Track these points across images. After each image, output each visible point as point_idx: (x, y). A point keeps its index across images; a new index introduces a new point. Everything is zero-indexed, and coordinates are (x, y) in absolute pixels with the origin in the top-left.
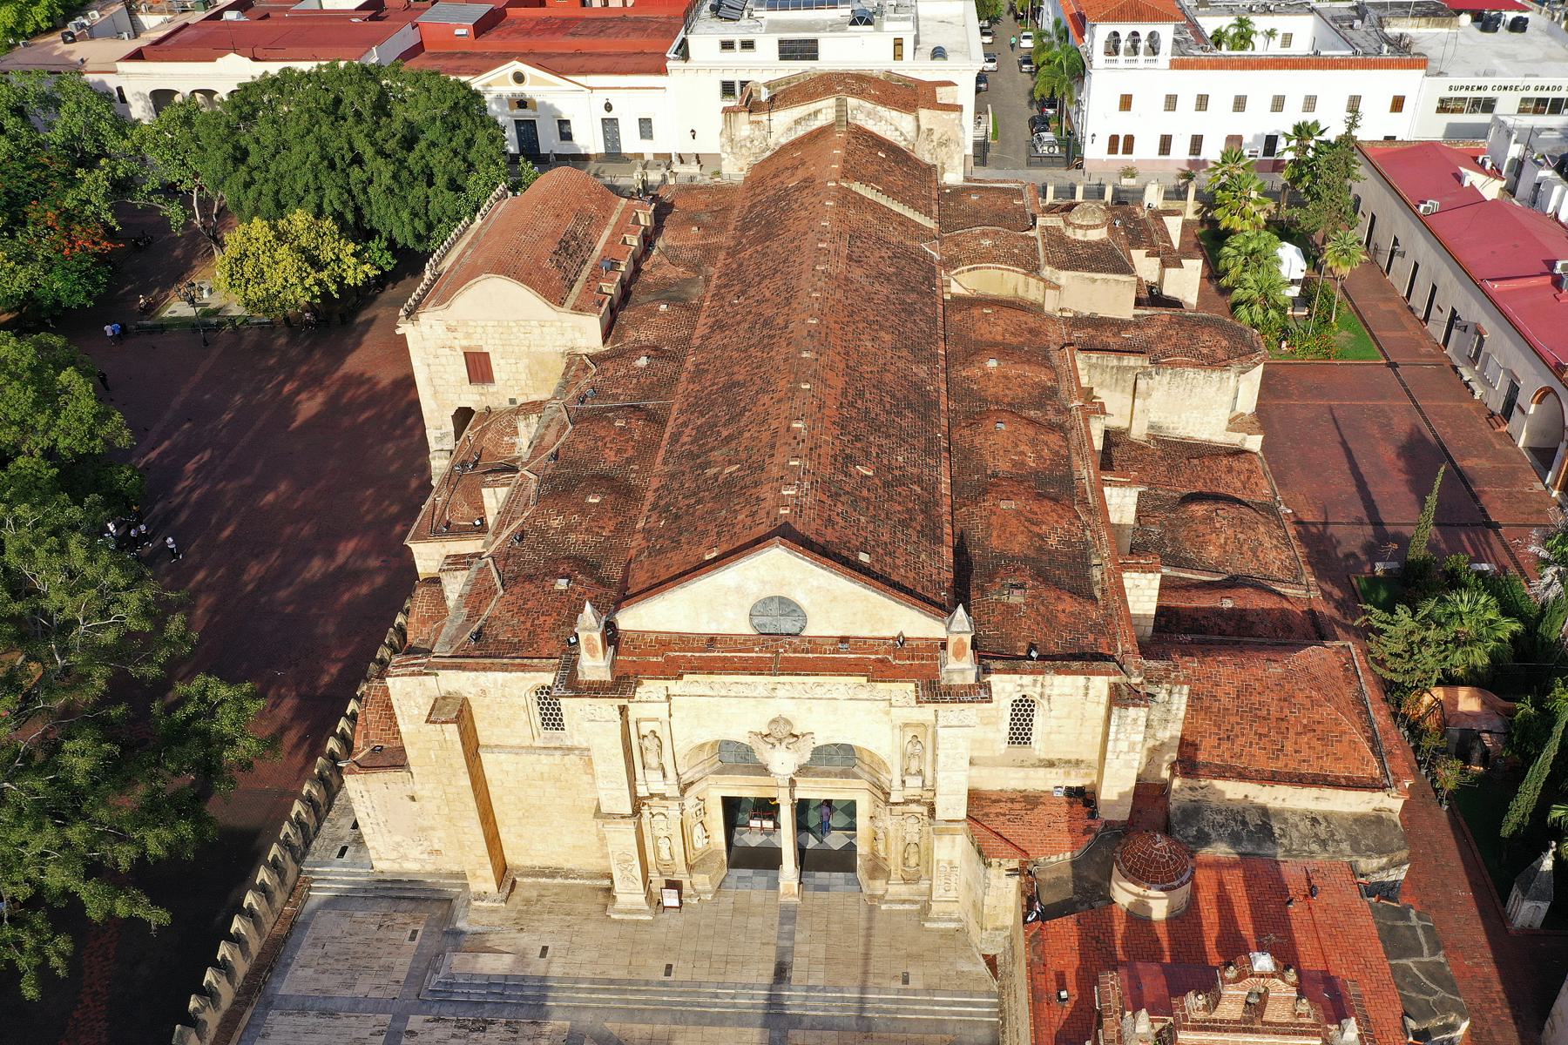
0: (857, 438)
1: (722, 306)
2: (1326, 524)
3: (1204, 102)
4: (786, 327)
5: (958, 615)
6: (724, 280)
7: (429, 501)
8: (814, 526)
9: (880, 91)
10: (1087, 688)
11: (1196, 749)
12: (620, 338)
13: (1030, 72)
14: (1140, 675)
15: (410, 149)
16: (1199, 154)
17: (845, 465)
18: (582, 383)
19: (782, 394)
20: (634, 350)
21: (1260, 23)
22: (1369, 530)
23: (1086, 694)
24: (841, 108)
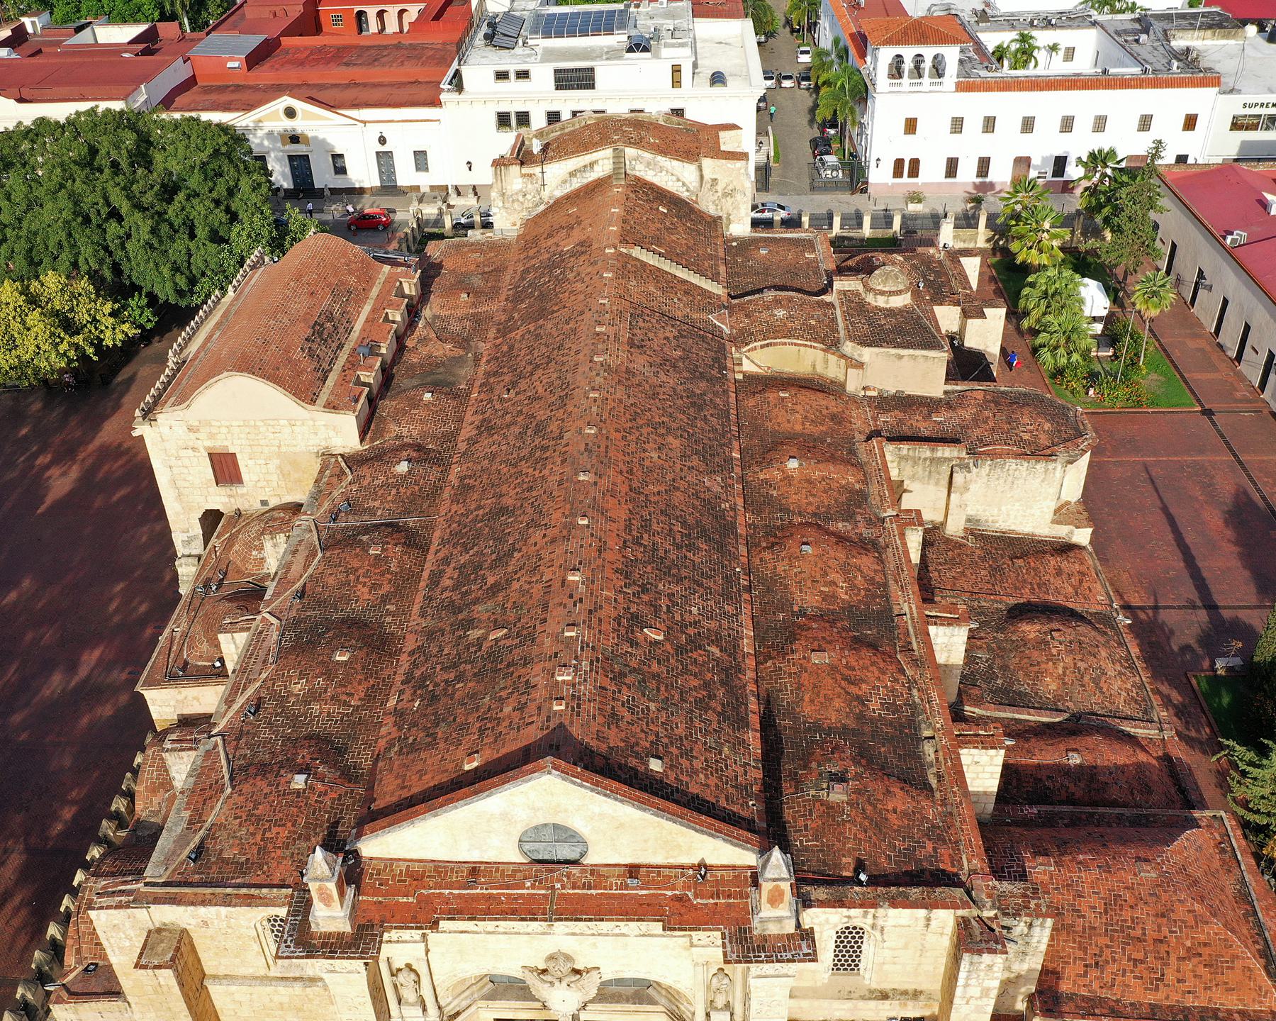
0: (644, 589)
1: (491, 401)
2: (1156, 608)
3: (991, 124)
4: (561, 438)
5: (773, 859)
6: (492, 367)
7: (167, 632)
8: (594, 727)
9: (659, 138)
10: (928, 919)
11: (1058, 978)
12: (379, 434)
13: (808, 89)
14: (993, 907)
15: (170, 201)
16: (986, 176)
17: (630, 629)
18: (336, 494)
19: (556, 531)
20: (396, 450)
21: (1042, 38)
22: (1202, 615)
23: (927, 926)
24: (619, 158)
